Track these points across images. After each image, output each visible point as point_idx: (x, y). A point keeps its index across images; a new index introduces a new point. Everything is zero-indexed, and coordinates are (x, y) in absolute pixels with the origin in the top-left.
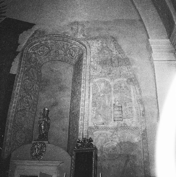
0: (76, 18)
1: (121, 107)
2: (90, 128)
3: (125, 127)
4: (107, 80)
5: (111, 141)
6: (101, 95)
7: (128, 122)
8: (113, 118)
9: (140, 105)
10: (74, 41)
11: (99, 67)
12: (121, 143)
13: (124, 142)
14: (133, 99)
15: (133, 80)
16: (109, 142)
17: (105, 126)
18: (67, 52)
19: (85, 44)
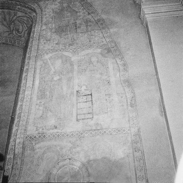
0: (49, 11)
1: (91, 95)
2: (32, 138)
3: (98, 130)
4: (66, 54)
5: (70, 159)
6: (55, 79)
7: (104, 120)
8: (75, 114)
9: (127, 90)
10: (18, 7)
11: (55, 37)
12: (89, 162)
13: (95, 160)
14: (113, 79)
15: (112, 49)
16: (65, 163)
17: (59, 131)
18: (12, 26)
19: (34, 7)
